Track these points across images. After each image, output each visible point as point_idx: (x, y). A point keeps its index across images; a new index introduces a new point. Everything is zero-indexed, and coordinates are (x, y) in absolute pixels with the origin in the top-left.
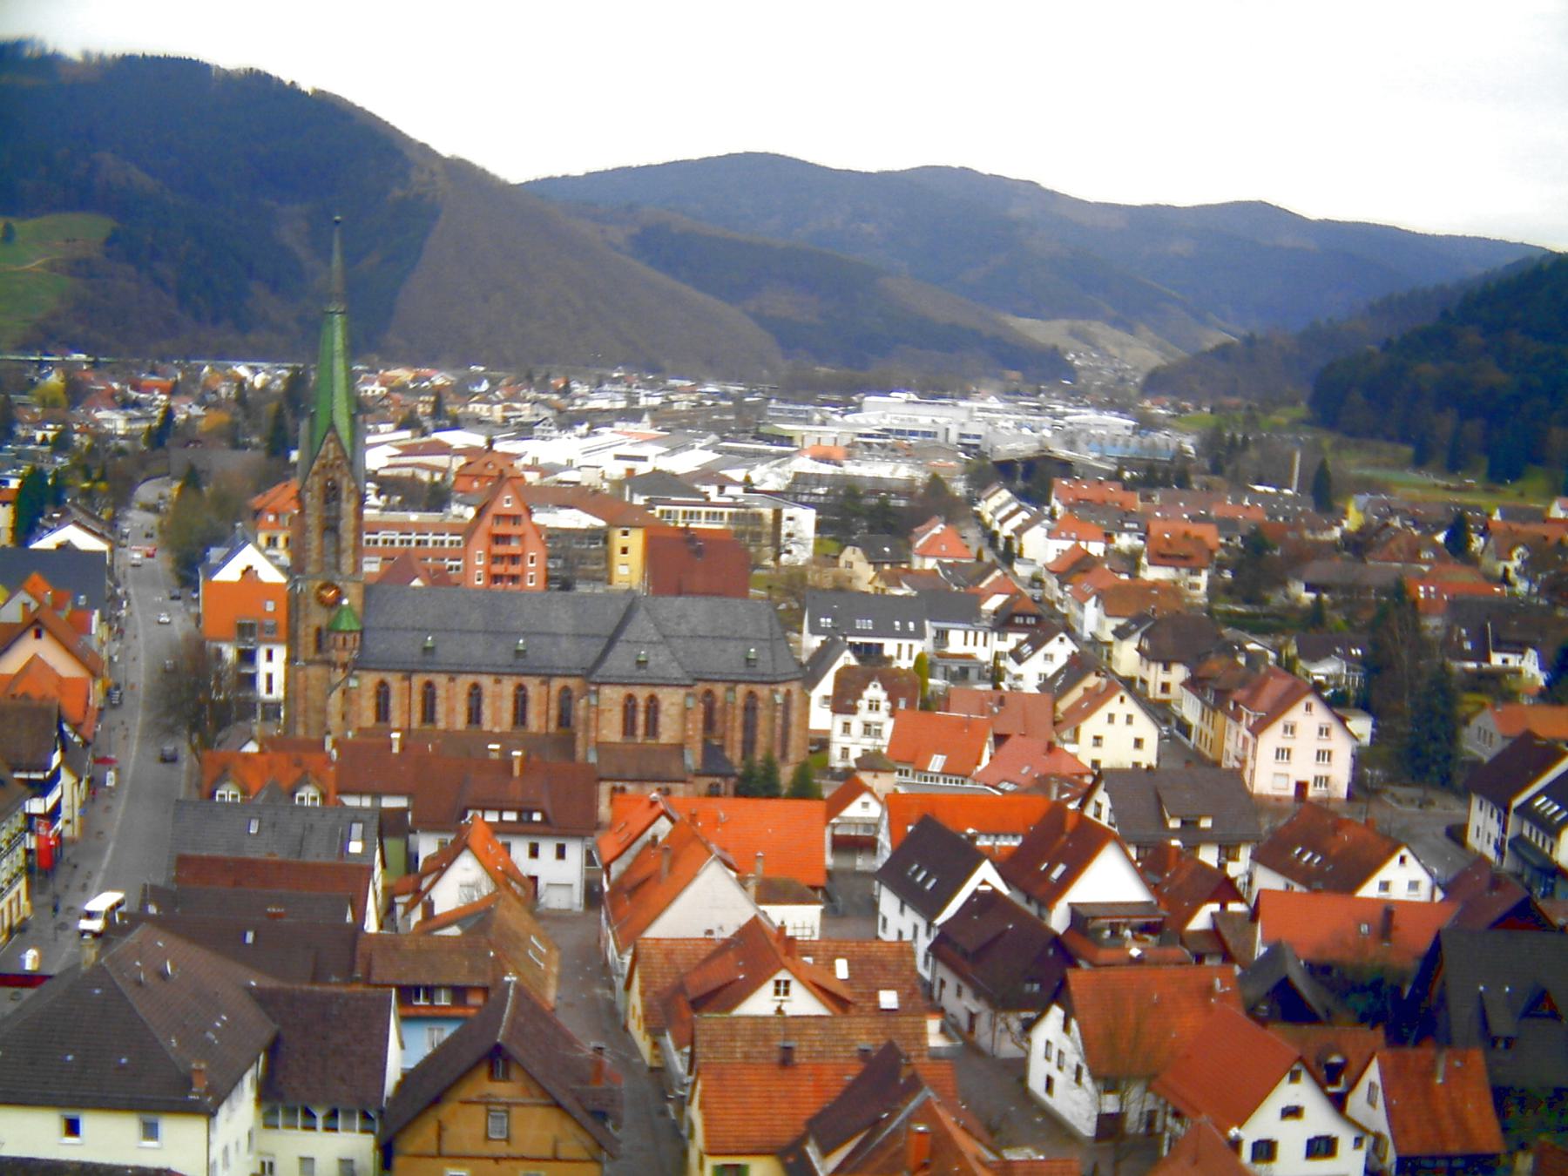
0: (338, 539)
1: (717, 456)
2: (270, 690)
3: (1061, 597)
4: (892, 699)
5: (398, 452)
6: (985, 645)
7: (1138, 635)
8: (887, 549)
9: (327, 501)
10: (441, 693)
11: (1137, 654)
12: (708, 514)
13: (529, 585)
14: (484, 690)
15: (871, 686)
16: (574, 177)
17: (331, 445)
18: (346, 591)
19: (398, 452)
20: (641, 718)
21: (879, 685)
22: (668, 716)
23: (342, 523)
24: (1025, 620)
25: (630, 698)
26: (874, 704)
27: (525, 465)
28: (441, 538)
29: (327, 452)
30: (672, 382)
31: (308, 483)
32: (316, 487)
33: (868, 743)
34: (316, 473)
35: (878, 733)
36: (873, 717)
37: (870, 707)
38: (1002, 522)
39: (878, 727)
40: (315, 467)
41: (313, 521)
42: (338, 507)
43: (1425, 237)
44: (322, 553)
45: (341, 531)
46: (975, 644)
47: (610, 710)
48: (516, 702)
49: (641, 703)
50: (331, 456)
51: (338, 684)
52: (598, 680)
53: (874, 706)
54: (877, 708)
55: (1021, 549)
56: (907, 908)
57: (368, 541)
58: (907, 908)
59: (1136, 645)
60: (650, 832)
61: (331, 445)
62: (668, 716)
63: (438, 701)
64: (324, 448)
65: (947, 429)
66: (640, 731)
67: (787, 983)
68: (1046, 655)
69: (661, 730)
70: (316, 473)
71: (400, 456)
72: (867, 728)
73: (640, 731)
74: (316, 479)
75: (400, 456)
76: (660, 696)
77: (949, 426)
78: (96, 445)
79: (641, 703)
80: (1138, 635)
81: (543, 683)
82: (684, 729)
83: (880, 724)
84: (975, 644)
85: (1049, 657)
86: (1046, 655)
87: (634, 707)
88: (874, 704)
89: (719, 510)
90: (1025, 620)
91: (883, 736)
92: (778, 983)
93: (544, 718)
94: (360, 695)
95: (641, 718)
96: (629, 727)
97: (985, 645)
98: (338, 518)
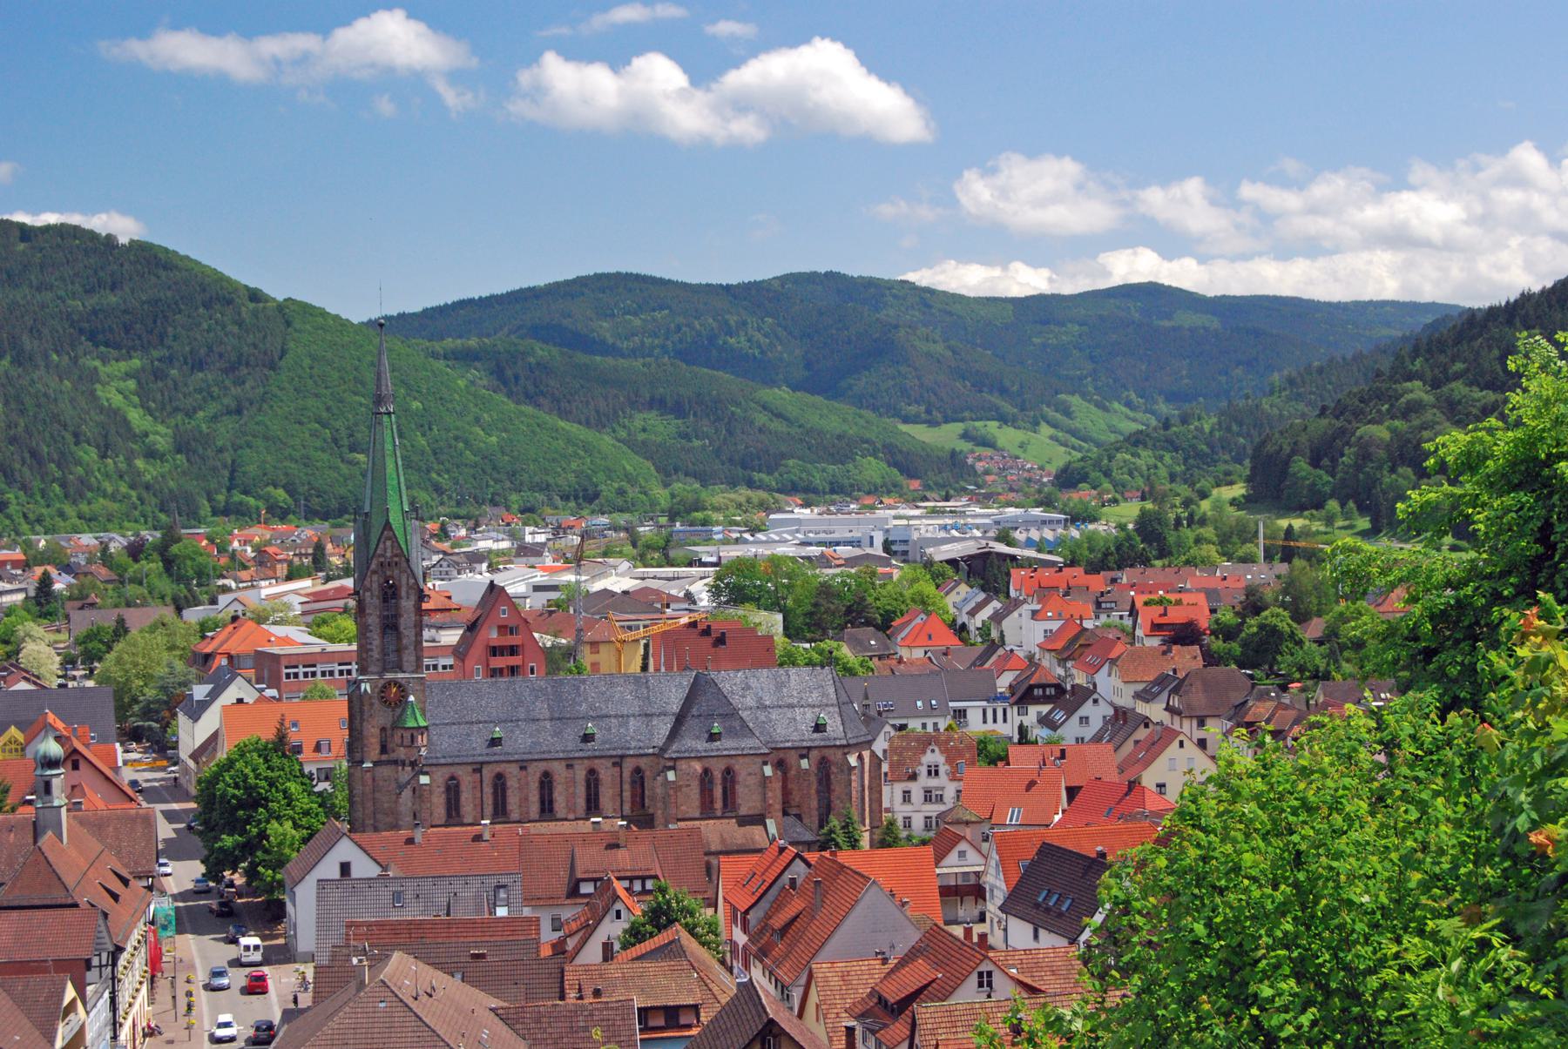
0: (399, 637)
3: (1063, 674)
4: (949, 761)
6: (1005, 721)
7: (1165, 694)
8: (873, 642)
9: (385, 600)
10: (512, 783)
11: (1167, 713)
14: (556, 777)
15: (929, 751)
16: (1424, 304)
17: (389, 543)
20: (718, 792)
21: (937, 749)
22: (747, 786)
23: (402, 621)
24: (1044, 692)
25: (706, 771)
26: (933, 769)
28: (349, 667)
29: (385, 550)
31: (367, 583)
32: (375, 586)
33: (933, 809)
34: (375, 572)
35: (940, 799)
36: (933, 782)
37: (929, 773)
38: (972, 613)
39: (939, 793)
40: (373, 566)
41: (373, 620)
42: (397, 607)
44: (384, 653)
45: (402, 629)
46: (995, 721)
47: (688, 786)
48: (588, 787)
49: (718, 775)
50: (389, 554)
51: (408, 783)
52: (674, 756)
53: (933, 772)
54: (937, 773)
55: (1002, 636)
56: (1042, 932)
57: (288, 676)
58: (1042, 932)
59: (1164, 706)
60: (787, 876)
61: (389, 543)
62: (747, 786)
63: (509, 793)
64: (381, 546)
65: (872, 538)
67: (990, 974)
68: (1081, 718)
69: (739, 801)
70: (375, 572)
72: (928, 796)
74: (375, 578)
76: (737, 767)
77: (873, 534)
79: (718, 775)
80: (1165, 694)
81: (614, 764)
82: (764, 799)
83: (943, 789)
84: (995, 721)
85: (1084, 720)
86: (1081, 718)
87: (711, 782)
88: (933, 769)
90: (1044, 692)
91: (945, 800)
92: (981, 975)
93: (618, 799)
94: (431, 792)
95: (718, 792)
97: (1005, 721)
98: (397, 616)
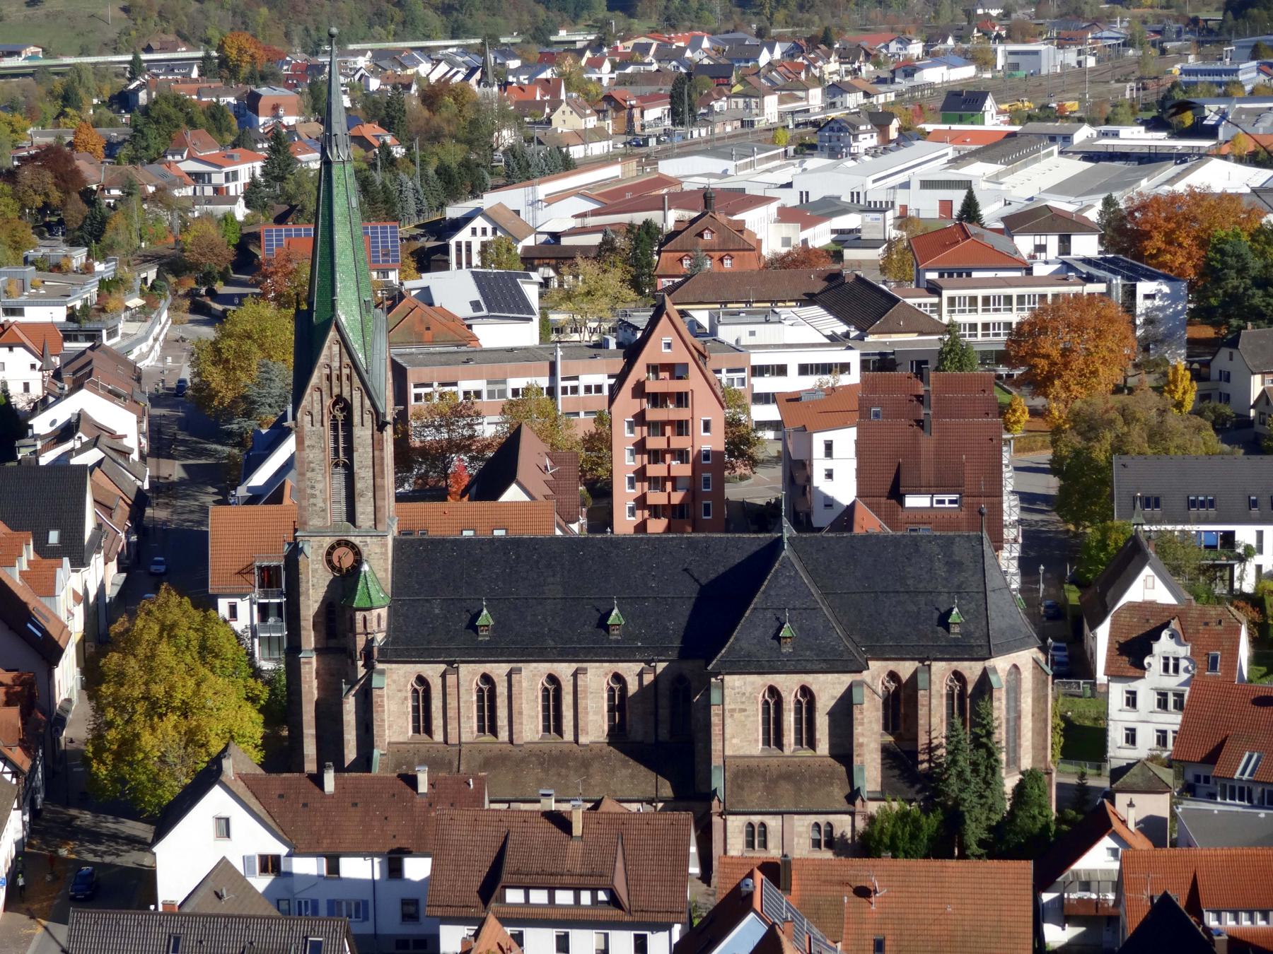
1: (1089, 165)
2: (845, 368)
5: (591, 206)
12: (986, 300)
13: (709, 475)
18: (365, 552)
19: (591, 206)
20: (789, 719)
27: (541, 296)
30: (351, 47)
43: (85, 624)
66: (789, 737)
71: (595, 213)
73: (789, 737)
75: (595, 213)
76: (814, 688)
78: (473, 156)
89: (1008, 291)
95: (789, 719)
96: (774, 734)
